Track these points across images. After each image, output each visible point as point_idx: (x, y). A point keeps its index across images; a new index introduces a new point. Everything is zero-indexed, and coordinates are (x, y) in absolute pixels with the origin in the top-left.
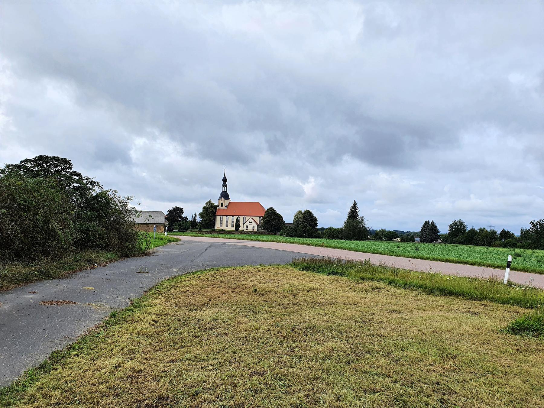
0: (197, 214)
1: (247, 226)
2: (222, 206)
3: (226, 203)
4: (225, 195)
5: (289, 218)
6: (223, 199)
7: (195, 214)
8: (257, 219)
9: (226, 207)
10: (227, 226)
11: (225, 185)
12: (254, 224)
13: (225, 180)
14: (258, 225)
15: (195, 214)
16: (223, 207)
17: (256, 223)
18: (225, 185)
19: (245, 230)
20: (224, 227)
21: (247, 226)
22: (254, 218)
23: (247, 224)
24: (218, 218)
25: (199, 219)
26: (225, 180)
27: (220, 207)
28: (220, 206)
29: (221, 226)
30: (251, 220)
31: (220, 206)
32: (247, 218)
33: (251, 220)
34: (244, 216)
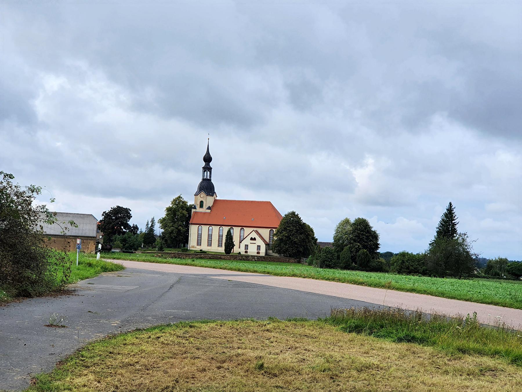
0: (156, 221)
1: (247, 246)
2: (201, 206)
3: (209, 201)
4: (207, 187)
6: (203, 194)
7: (153, 221)
8: (265, 233)
9: (209, 208)
10: (210, 244)
11: (207, 168)
12: (259, 242)
13: (208, 159)
14: (267, 245)
15: (153, 221)
16: (204, 210)
17: (264, 240)
18: (207, 168)
19: (243, 253)
20: (204, 247)
21: (247, 246)
22: (260, 230)
23: (247, 241)
24: (193, 230)
25: (158, 230)
26: (208, 159)
27: (199, 210)
28: (198, 207)
29: (199, 243)
31: (198, 207)
32: (247, 230)
34: (232, 226)
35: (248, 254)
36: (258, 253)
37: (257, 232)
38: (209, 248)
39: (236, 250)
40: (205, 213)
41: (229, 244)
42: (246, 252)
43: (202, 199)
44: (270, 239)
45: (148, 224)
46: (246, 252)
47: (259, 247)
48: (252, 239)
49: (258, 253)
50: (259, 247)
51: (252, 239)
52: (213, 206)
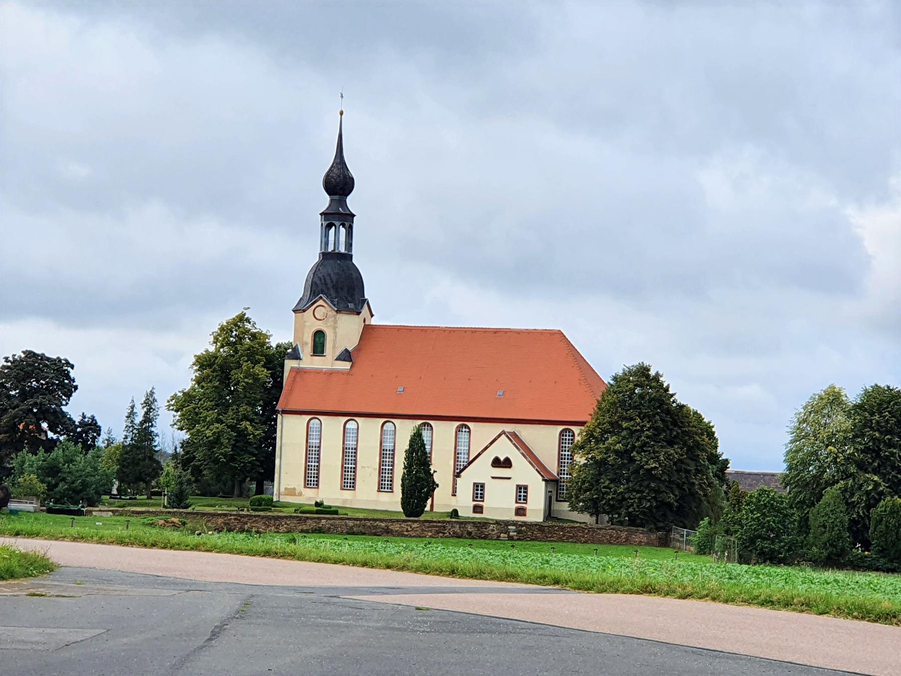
1: (479, 489)
5: (502, 459)
7: (149, 403)
8: (545, 441)
9: (346, 356)
12: (523, 472)
13: (339, 184)
20: (330, 492)
21: (479, 489)
26: (339, 184)
30: (505, 449)
33: (505, 449)
35: (486, 515)
36: (520, 512)
37: (515, 438)
38: (347, 494)
39: (442, 501)
40: (331, 373)
41: (419, 484)
42: (478, 509)
43: (319, 326)
44: (560, 464)
45: (131, 414)
46: (478, 509)
47: (522, 491)
48: (497, 463)
49: (520, 512)
50: (522, 491)
51: (497, 463)
52: (358, 349)
